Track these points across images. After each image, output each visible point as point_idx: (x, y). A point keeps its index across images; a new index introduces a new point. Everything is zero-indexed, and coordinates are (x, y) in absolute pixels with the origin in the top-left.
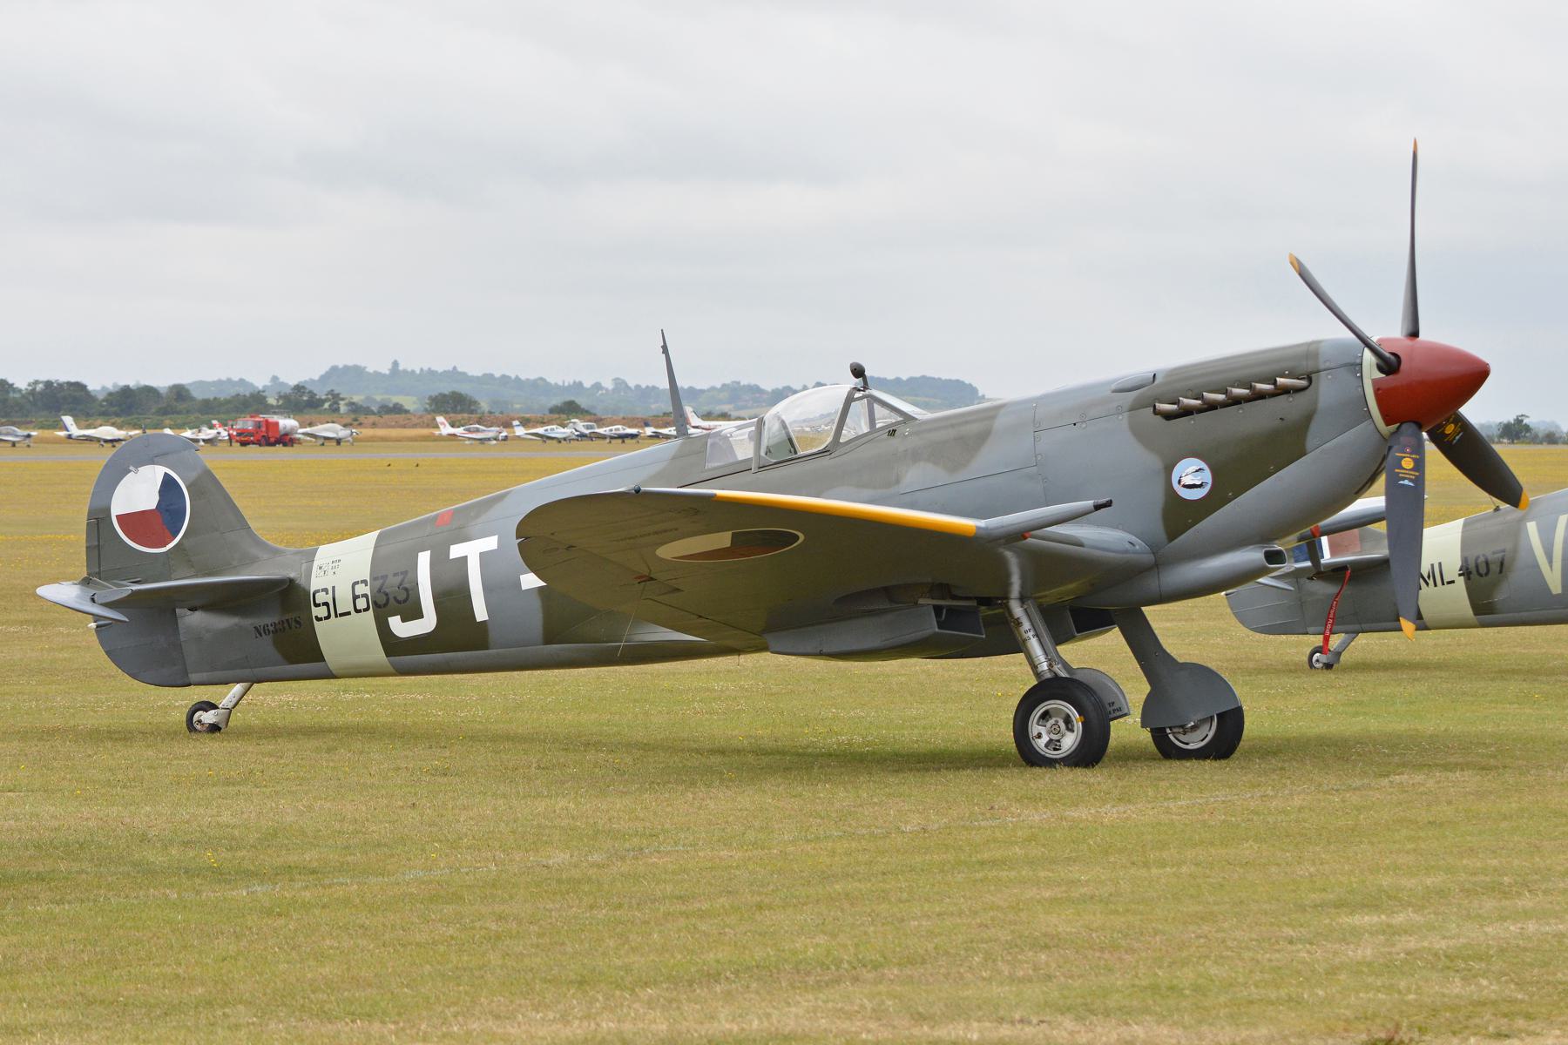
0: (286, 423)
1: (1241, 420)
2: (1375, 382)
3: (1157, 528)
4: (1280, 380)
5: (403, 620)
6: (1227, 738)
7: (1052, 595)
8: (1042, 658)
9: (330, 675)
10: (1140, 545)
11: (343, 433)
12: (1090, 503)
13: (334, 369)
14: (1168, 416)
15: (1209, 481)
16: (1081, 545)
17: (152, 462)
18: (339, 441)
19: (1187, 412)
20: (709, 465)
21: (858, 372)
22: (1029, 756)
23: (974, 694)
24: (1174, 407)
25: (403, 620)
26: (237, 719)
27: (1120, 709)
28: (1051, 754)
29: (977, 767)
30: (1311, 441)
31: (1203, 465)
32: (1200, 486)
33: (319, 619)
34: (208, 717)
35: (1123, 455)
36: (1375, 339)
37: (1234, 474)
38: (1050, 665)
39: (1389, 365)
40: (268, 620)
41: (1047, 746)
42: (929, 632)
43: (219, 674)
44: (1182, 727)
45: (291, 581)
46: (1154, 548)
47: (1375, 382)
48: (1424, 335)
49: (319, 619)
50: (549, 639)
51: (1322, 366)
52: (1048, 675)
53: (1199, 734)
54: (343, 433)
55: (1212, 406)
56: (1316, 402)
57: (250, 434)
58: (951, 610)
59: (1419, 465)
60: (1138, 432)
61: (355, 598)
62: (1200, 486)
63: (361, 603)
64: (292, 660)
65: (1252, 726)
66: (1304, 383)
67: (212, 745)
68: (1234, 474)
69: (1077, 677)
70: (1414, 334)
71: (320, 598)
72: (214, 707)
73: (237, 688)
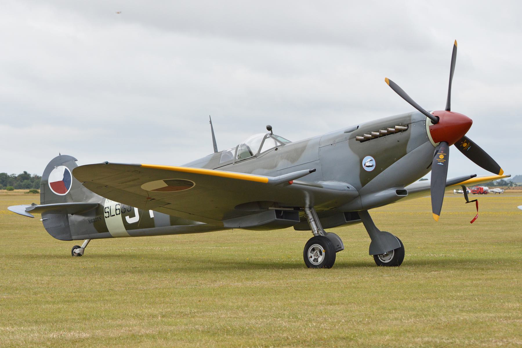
0: (485, 188)
1: (384, 142)
2: (430, 127)
3: (358, 181)
4: (397, 127)
5: (130, 217)
6: (398, 259)
7: (319, 208)
8: (316, 229)
9: (111, 237)
10: (352, 187)
11: (501, 191)
12: (308, 170)
13: (517, 176)
14: (362, 141)
15: (374, 164)
16: (322, 187)
17: (61, 164)
18: (499, 193)
19: (367, 139)
20: (221, 162)
21: (269, 128)
22: (308, 265)
23: (290, 241)
24: (364, 139)
25: (130, 217)
26: (85, 253)
27: (340, 248)
28: (315, 263)
29: (268, 268)
30: (408, 149)
31: (372, 159)
32: (372, 166)
33: (106, 217)
34: (77, 251)
35: (347, 154)
36: (431, 113)
37: (383, 163)
38: (318, 231)
39: (435, 120)
40: (92, 218)
41: (314, 261)
42: (273, 220)
43: (80, 236)
44: (382, 254)
45: (99, 204)
46: (358, 189)
47: (430, 127)
48: (452, 110)
49: (106, 217)
50: (172, 224)
51: (412, 122)
52: (317, 235)
53: (388, 257)
54: (501, 191)
55: (376, 137)
56: (409, 135)
57: (475, 191)
58: (285, 212)
59: (446, 158)
60: (351, 146)
61: (116, 210)
62: (372, 166)
63: (118, 212)
64: (100, 232)
65: (408, 256)
66: (406, 128)
67: (79, 259)
68: (383, 163)
69: (327, 236)
70: (448, 109)
71: (107, 210)
72: (79, 247)
73: (86, 241)
